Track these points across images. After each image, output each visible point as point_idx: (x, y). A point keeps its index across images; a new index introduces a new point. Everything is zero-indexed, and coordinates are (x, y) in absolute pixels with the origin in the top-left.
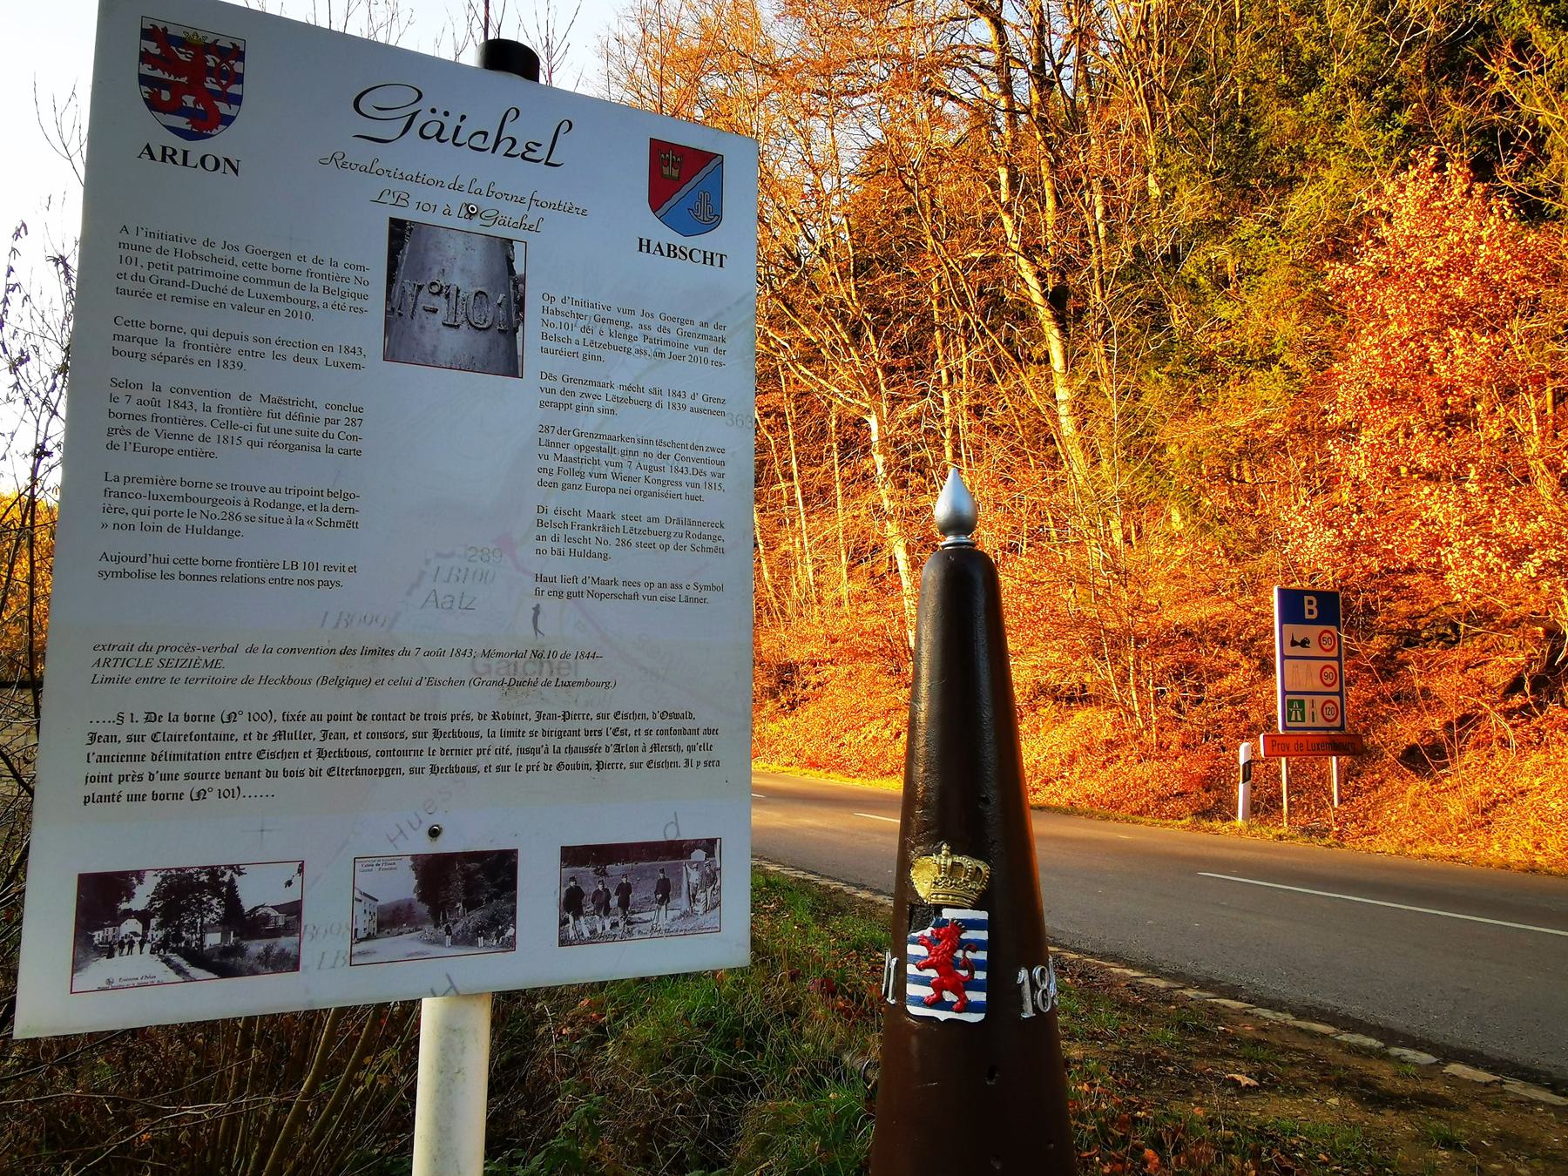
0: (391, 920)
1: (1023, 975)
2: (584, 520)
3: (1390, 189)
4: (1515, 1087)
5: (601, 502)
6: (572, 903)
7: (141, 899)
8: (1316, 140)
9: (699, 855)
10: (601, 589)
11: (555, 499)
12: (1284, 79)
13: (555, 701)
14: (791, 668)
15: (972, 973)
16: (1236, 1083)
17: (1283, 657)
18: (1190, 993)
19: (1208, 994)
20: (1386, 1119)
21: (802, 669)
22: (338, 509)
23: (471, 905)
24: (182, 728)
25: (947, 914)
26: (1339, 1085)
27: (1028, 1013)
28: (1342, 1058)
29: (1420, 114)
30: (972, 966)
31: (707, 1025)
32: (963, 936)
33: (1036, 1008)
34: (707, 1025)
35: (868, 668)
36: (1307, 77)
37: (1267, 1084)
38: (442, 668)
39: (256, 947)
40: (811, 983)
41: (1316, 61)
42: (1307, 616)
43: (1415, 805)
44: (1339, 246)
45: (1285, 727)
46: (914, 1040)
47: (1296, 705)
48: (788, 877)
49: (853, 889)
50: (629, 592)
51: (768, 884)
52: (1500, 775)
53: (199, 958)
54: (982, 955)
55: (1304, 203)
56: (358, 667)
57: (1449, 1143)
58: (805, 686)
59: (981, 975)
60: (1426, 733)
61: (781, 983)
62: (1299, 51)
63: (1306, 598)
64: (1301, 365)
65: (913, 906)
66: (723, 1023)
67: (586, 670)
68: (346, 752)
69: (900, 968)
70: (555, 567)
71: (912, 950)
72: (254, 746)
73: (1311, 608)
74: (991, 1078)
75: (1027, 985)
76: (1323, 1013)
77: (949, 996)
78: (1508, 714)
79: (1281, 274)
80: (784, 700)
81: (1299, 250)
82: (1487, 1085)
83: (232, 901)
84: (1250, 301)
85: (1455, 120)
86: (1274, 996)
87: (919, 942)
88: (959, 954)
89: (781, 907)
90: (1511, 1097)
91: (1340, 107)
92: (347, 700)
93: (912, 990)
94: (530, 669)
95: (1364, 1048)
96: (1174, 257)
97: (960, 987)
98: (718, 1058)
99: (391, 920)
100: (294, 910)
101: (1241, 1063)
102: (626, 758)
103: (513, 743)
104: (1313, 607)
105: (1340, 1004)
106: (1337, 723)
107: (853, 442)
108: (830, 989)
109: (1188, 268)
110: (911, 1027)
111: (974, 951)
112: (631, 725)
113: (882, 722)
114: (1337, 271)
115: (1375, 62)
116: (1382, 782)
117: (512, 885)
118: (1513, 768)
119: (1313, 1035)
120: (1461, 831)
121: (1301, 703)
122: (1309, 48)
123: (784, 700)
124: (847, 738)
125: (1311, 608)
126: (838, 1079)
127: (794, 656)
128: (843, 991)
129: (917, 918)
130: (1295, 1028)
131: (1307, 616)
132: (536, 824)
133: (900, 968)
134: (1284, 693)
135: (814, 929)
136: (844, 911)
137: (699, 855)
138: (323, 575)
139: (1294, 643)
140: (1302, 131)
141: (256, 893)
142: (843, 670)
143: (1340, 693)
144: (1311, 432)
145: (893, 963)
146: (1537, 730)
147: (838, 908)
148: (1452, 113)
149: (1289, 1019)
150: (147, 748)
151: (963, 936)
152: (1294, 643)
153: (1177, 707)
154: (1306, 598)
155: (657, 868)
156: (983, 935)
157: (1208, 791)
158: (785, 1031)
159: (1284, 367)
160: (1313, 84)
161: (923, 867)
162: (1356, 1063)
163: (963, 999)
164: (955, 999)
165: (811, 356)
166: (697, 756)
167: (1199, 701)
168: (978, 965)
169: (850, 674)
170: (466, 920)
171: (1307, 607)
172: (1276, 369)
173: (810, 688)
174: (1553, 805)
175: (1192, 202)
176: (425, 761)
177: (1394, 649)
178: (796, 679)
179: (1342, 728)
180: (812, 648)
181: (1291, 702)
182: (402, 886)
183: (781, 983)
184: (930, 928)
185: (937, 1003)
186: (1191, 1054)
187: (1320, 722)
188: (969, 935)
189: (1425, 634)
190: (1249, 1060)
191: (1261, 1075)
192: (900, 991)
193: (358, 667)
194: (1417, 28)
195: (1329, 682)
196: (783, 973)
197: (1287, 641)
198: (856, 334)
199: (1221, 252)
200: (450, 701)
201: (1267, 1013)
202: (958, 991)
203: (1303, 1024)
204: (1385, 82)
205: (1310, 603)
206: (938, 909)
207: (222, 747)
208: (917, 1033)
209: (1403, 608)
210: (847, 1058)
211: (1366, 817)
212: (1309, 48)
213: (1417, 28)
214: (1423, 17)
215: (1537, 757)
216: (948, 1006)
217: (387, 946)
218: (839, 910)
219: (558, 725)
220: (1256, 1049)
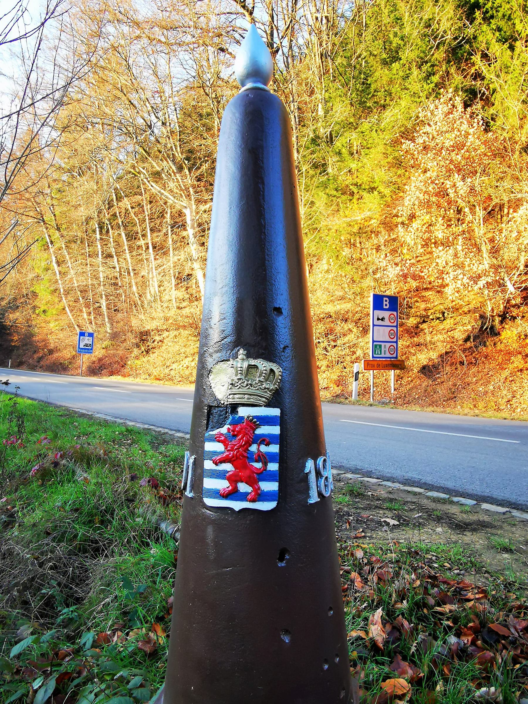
1: (310, 465)
3: (432, 107)
4: (515, 513)
8: (397, 86)
12: (384, 56)
14: (147, 333)
15: (265, 464)
16: (388, 524)
17: (374, 325)
18: (349, 476)
19: (359, 476)
20: (468, 537)
21: (152, 333)
25: (243, 412)
26: (439, 520)
27: (314, 498)
28: (432, 505)
29: (442, 78)
31: (76, 510)
32: (258, 431)
33: (320, 494)
34: (76, 510)
35: (185, 333)
36: (394, 57)
37: (404, 523)
40: (143, 482)
41: (399, 48)
42: (385, 307)
43: (426, 391)
44: (408, 134)
45: (373, 357)
46: (210, 531)
47: (378, 347)
48: (139, 427)
49: (173, 432)
51: (127, 430)
52: (460, 377)
54: (274, 449)
55: (390, 116)
57: (506, 550)
58: (154, 341)
59: (273, 467)
60: (430, 360)
61: (125, 481)
62: (391, 43)
63: (385, 299)
64: (387, 192)
65: (210, 407)
66: (86, 509)
69: (198, 464)
71: (210, 446)
73: (386, 303)
74: (281, 559)
75: (313, 473)
76: (414, 482)
77: (243, 487)
78: (464, 351)
79: (381, 148)
80: (143, 349)
81: (388, 136)
82: (504, 513)
84: (365, 161)
85: (456, 83)
86: (389, 475)
87: (217, 439)
88: (254, 448)
89: (134, 442)
90: (518, 519)
91: (408, 72)
93: (209, 483)
95: (441, 499)
96: (331, 140)
98: (81, 531)
101: (386, 512)
104: (387, 303)
105: (420, 477)
106: (395, 355)
107: (179, 224)
108: (154, 484)
109: (338, 144)
110: (205, 518)
111: (267, 444)
113: (191, 359)
114: (407, 145)
115: (424, 52)
116: (412, 381)
118: (465, 374)
119: (415, 494)
120: (444, 401)
121: (380, 346)
122: (396, 41)
123: (143, 349)
124: (174, 366)
125: (386, 303)
126: (157, 540)
127: (148, 327)
128: (164, 484)
129: (214, 418)
130: (405, 491)
131: (385, 307)
133: (198, 464)
134: (373, 341)
135: (151, 453)
136: (168, 443)
139: (378, 319)
140: (391, 82)
142: (173, 333)
143: (396, 342)
144: (389, 226)
145: (191, 461)
146: (474, 357)
147: (165, 441)
148: (455, 80)
149: (402, 487)
151: (258, 431)
152: (378, 319)
153: (325, 349)
154: (385, 299)
156: (276, 430)
157: (338, 386)
158: (126, 511)
159: (380, 193)
160: (396, 59)
161: (220, 371)
162: (440, 506)
163: (257, 490)
164: (249, 489)
165: (157, 175)
167: (335, 346)
169: (176, 336)
171: (385, 303)
172: (376, 193)
173: (156, 343)
174: (481, 389)
175: (342, 110)
177: (419, 323)
178: (149, 338)
179: (396, 357)
181: (376, 346)
183: (125, 481)
184: (226, 427)
185: (232, 494)
186: (360, 508)
187: (388, 355)
188: (263, 430)
189: (431, 317)
190: (390, 509)
191: (398, 517)
192: (197, 485)
194: (443, 37)
195: (392, 337)
196: (126, 475)
197: (375, 319)
198: (180, 169)
199: (353, 136)
201: (389, 484)
202: (252, 482)
203: (409, 489)
204: (426, 62)
205: (386, 301)
206: (234, 407)
208: (213, 522)
209: (423, 306)
210: (163, 526)
211: (405, 396)
212: (396, 41)
213: (443, 37)
214: (445, 32)
215: (474, 369)
216: (243, 497)
218: (165, 442)
220: (390, 502)
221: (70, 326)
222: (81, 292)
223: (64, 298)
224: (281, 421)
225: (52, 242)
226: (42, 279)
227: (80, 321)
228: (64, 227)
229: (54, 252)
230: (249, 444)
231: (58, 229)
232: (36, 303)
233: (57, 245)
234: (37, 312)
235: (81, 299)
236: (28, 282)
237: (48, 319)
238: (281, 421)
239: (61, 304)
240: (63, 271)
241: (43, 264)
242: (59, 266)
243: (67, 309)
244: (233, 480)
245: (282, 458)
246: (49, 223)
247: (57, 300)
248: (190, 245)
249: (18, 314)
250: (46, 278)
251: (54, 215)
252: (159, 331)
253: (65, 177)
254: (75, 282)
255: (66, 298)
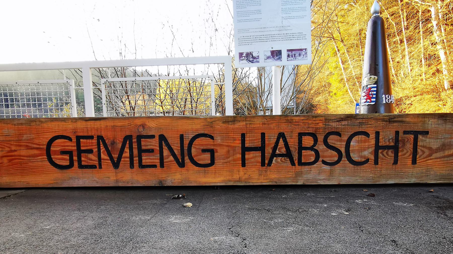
0: (268, 58)
2: (288, 9)
5: (289, 6)
6: (288, 56)
7: (244, 55)
9: (304, 50)
10: (290, 18)
11: (284, 7)
13: (285, 32)
22: (259, 12)
23: (277, 56)
24: (246, 37)
30: (372, 95)
38: (271, 29)
39: (255, 60)
50: (294, 18)
53: (250, 61)
56: (263, 30)
59: (374, 96)
67: (289, 28)
68: (261, 39)
70: (284, 16)
72: (253, 39)
77: (368, 100)
83: (252, 56)
88: (370, 93)
92: (262, 34)
94: (282, 28)
97: (370, 98)
99: (268, 58)
100: (258, 56)
102: (294, 39)
103: (280, 37)
112: (294, 35)
117: (281, 54)
132: (284, 47)
137: (304, 50)
138: (258, 20)
141: (254, 55)
142: (418, 98)
150: (243, 40)
155: (298, 52)
156: (375, 89)
166: (303, 38)
168: (374, 94)
170: (276, 58)
176: (271, 40)
180: (407, 92)
182: (269, 54)
193: (263, 30)
200: (273, 33)
207: (250, 39)
217: (268, 60)
219: (286, 35)
221: (351, 102)
222: (357, 78)
223: (346, 84)
224: (377, 87)
225: (339, 50)
226: (334, 74)
227: (357, 97)
228: (346, 39)
229: (340, 56)
230: (369, 92)
231: (342, 41)
232: (331, 90)
233: (341, 52)
234: (331, 94)
235: (357, 83)
236: (326, 77)
237: (337, 98)
238: (377, 87)
239: (345, 88)
240: (345, 67)
241: (334, 65)
242: (343, 64)
243: (349, 90)
244: (367, 99)
245: (377, 94)
246: (337, 38)
247: (342, 86)
248: (434, 33)
249: (320, 97)
250: (336, 72)
251: (340, 33)
252: (408, 97)
253: (346, 7)
254: (353, 72)
255: (348, 84)
